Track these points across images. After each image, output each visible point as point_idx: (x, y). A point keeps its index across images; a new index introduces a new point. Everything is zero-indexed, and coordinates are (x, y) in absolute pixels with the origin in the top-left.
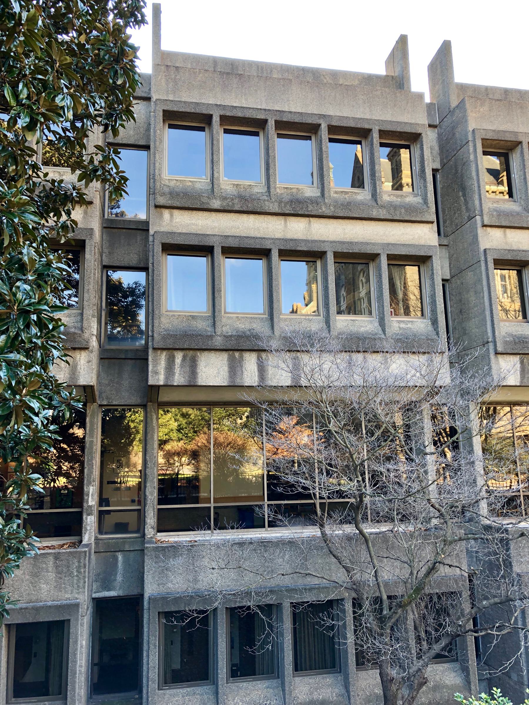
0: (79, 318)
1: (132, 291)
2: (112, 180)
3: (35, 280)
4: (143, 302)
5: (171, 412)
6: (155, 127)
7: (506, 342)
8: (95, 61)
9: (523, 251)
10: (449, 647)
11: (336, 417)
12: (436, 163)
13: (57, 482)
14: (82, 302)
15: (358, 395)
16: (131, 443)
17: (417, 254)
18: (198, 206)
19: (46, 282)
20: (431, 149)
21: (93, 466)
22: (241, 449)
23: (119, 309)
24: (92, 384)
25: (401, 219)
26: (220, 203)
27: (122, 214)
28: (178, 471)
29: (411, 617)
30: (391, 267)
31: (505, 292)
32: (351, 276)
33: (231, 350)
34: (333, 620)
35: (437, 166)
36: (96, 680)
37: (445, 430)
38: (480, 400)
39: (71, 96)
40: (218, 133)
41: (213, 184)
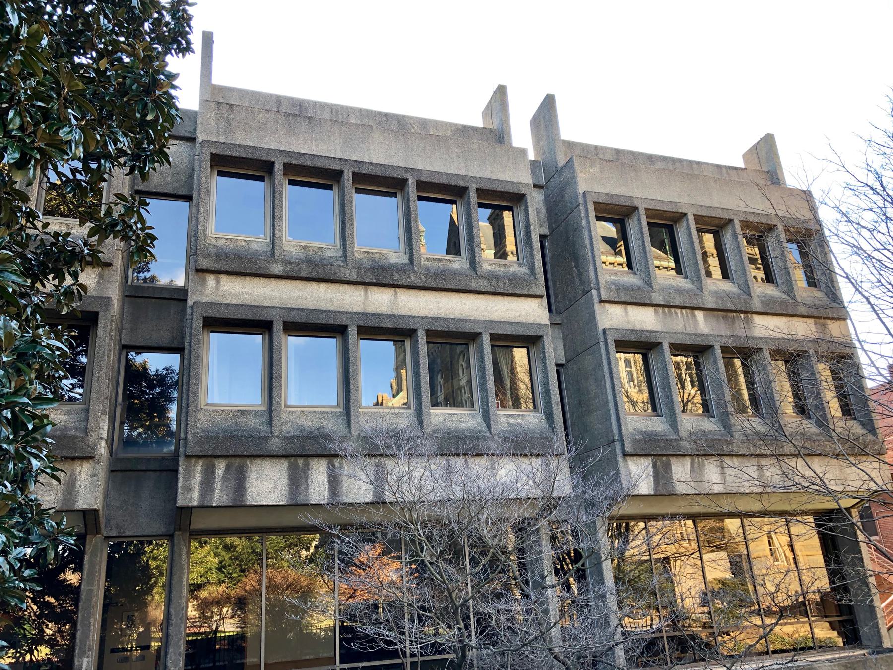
1: (161, 379)
2: (134, 238)
3: (13, 363)
5: (210, 544)
6: (200, 174)
7: (635, 441)
8: (118, 91)
9: (648, 331)
11: (430, 543)
12: (544, 228)
13: (35, 653)
14: (88, 394)
15: (457, 511)
16: (149, 590)
17: (525, 333)
18: (253, 271)
19: (29, 366)
20: (538, 212)
21: (89, 627)
22: (306, 594)
23: (142, 403)
24: (96, 507)
25: (505, 292)
26: (282, 268)
27: (153, 279)
28: (217, 628)
30: (496, 349)
32: (449, 359)
33: (292, 456)
35: (545, 231)
37: (568, 553)
38: (607, 514)
39: (82, 129)
40: (281, 184)
41: (273, 244)
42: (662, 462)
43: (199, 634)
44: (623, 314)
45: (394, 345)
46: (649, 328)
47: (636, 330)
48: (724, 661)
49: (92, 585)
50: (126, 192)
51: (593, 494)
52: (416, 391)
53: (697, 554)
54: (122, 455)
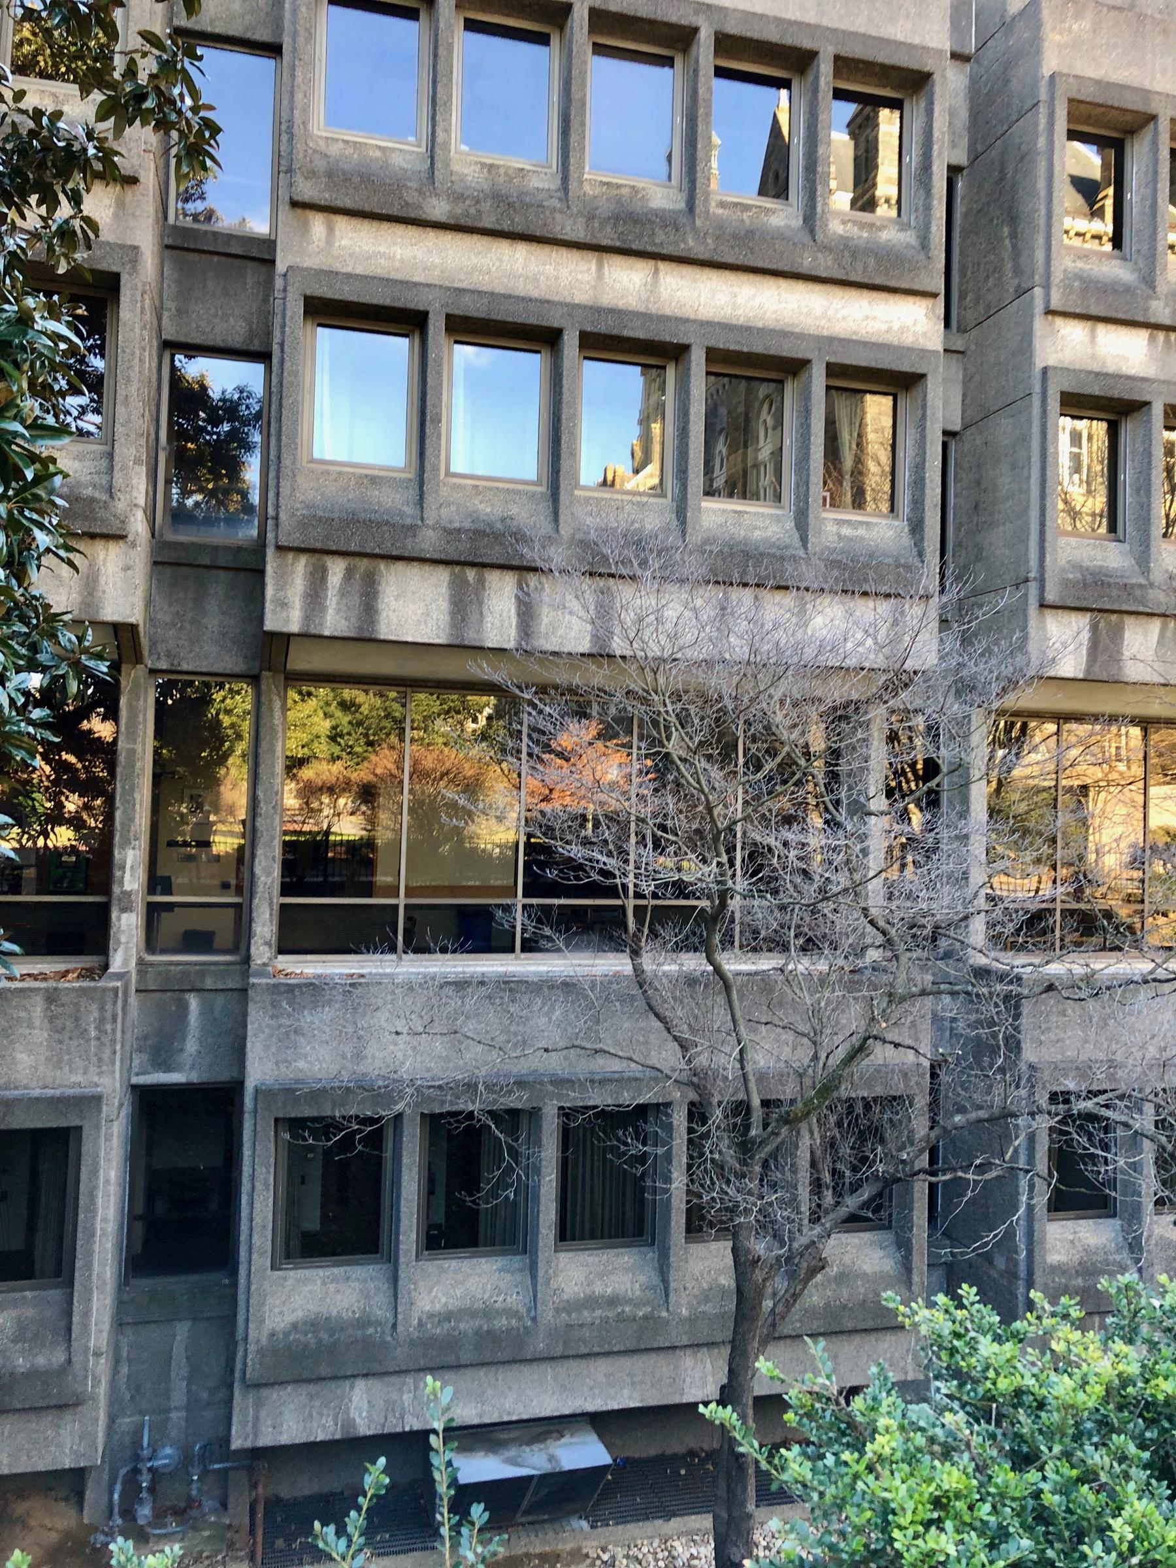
0: (104, 463)
1: (230, 409)
4: (256, 438)
7: (1066, 583)
9: (1128, 378)
10: (876, 1204)
15: (736, 679)
16: (223, 759)
19: (17, 365)
20: (951, 115)
22: (472, 788)
24: (133, 620)
25: (866, 280)
27: (210, 215)
28: (329, 827)
29: (805, 1142)
30: (833, 392)
31: (1077, 469)
32: (741, 409)
33: (458, 563)
34: (644, 1144)
36: (138, 1249)
37: (913, 765)
40: (449, 26)
41: (432, 158)
42: (1108, 623)
43: (300, 833)
44: (1087, 340)
45: (643, 374)
46: (1132, 372)
47: (1106, 375)
48: (1152, 954)
49: (134, 741)
50: (159, 29)
51: (975, 669)
52: (679, 465)
53: (1141, 784)
54: (170, 537)
